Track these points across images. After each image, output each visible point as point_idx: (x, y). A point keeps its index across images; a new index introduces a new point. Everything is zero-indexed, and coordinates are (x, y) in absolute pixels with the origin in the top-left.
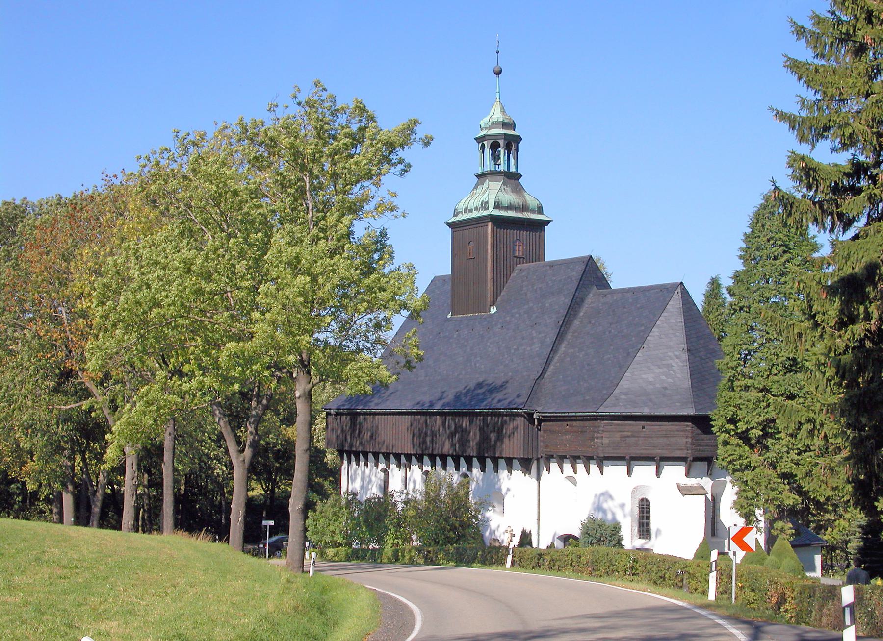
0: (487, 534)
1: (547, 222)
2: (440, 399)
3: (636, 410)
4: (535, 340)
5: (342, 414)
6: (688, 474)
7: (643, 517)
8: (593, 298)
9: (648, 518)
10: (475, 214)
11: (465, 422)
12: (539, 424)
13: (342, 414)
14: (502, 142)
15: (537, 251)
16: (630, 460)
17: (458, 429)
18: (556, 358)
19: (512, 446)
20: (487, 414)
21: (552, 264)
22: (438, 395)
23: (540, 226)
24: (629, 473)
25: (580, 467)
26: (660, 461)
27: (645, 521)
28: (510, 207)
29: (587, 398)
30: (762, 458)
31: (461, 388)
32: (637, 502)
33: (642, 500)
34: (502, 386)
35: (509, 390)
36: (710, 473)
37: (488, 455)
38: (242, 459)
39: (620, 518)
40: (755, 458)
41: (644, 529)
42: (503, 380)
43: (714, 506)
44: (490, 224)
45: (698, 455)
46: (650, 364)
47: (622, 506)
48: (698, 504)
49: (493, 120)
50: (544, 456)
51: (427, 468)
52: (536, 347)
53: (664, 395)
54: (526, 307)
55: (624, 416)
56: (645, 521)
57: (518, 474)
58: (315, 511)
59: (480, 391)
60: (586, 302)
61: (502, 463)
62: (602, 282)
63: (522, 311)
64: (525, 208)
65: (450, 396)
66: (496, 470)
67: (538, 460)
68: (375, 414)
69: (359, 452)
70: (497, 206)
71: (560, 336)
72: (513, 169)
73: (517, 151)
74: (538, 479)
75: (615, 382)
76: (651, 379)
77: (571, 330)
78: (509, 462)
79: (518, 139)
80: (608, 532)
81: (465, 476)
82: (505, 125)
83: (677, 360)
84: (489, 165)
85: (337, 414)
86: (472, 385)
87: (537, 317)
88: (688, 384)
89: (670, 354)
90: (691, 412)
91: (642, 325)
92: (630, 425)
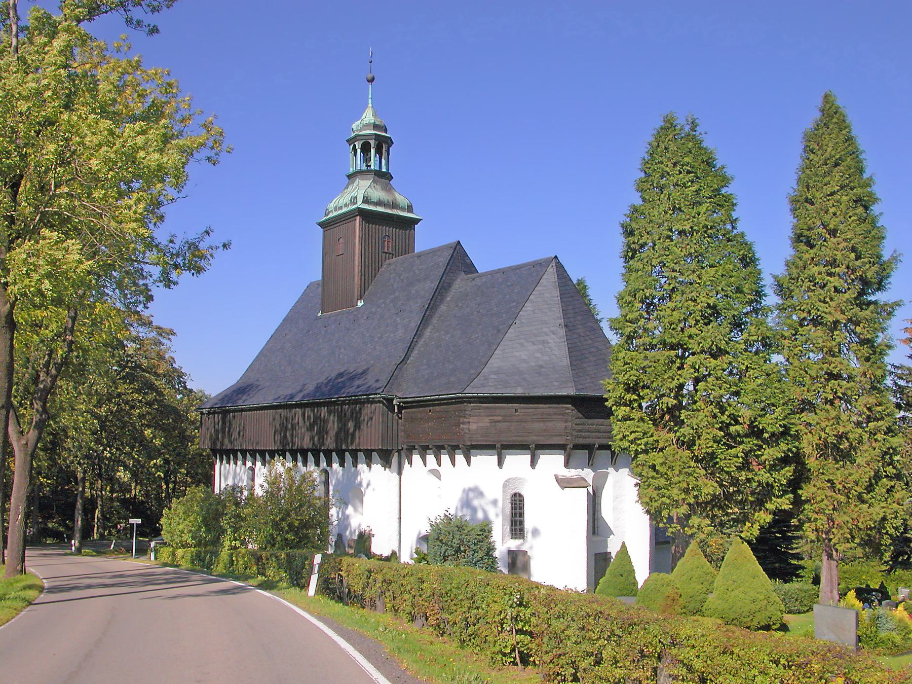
0: (348, 533)
1: (417, 221)
2: (301, 391)
3: (508, 390)
4: (399, 326)
5: (214, 413)
6: (567, 465)
7: (516, 514)
8: (461, 283)
9: (521, 515)
10: (345, 210)
11: (324, 411)
12: (400, 412)
13: (214, 413)
14: (372, 142)
15: (407, 247)
16: (500, 448)
17: (317, 418)
18: (421, 343)
19: (370, 434)
20: (343, 403)
21: (419, 256)
22: (299, 388)
23: (411, 224)
24: (500, 463)
25: (445, 458)
26: (535, 449)
27: (518, 518)
28: (379, 203)
29: (452, 379)
30: (672, 435)
31: (322, 379)
32: (509, 497)
33: (515, 495)
34: (364, 372)
35: (369, 377)
36: (591, 464)
37: (347, 450)
38: (24, 442)
39: (492, 516)
40: (664, 436)
41: (517, 527)
42: (365, 368)
43: (594, 501)
44: (358, 218)
45: (581, 441)
46: (522, 341)
47: (495, 502)
48: (580, 497)
49: (364, 122)
50: (405, 447)
51: (289, 464)
52: (400, 333)
53: (539, 374)
54: (392, 296)
55: (493, 397)
56: (518, 518)
57: (377, 468)
58: (170, 509)
59: (340, 380)
60: (453, 287)
61: (361, 455)
62: (470, 268)
63: (388, 301)
64: (395, 206)
65: (311, 387)
66: (355, 465)
67: (399, 451)
68: (242, 410)
69: (237, 451)
70: (366, 200)
71: (425, 321)
72: (384, 170)
73: (388, 154)
74: (400, 473)
75: (484, 360)
76: (524, 357)
77: (437, 315)
78: (368, 454)
79: (389, 142)
80: (472, 538)
81: (326, 472)
82: (376, 126)
83: (552, 336)
84: (360, 165)
85: (209, 413)
86: (333, 375)
87: (402, 304)
88: (566, 362)
89: (545, 330)
90: (572, 392)
91: (515, 301)
92: (501, 408)
